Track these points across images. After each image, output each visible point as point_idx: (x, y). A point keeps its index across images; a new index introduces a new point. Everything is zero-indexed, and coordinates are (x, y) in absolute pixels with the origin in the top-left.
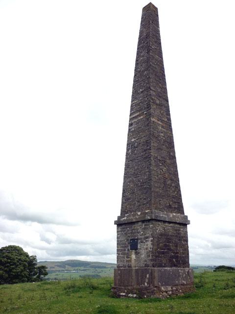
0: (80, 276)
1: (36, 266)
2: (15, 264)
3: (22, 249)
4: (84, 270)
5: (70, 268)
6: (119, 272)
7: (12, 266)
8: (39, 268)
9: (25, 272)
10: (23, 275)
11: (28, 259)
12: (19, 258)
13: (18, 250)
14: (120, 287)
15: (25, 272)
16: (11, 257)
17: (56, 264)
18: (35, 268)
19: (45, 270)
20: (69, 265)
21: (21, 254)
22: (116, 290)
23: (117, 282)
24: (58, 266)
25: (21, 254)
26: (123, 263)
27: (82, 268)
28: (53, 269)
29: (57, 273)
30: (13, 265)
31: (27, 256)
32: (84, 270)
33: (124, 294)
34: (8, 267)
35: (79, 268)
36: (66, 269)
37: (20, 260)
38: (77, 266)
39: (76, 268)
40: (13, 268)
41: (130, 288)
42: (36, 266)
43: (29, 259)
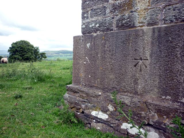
0: (68, 59)
1: (39, 53)
2: (25, 52)
3: (29, 43)
4: (70, 56)
5: (62, 54)
6: (88, 45)
7: (24, 53)
8: (41, 54)
9: (33, 56)
10: (31, 58)
11: (33, 49)
12: (28, 48)
13: (26, 43)
14: (91, 91)
15: (33, 56)
16: (23, 48)
17: (54, 52)
18: (38, 54)
19: (45, 55)
20: (62, 53)
21: (29, 46)
22: (77, 98)
23: (82, 75)
24: (55, 53)
25: (29, 46)
26: (100, 18)
27: (69, 54)
28: (53, 55)
29: (55, 57)
30: (24, 52)
31: (33, 47)
32: (70, 56)
33: (104, 116)
34: (21, 53)
35: (67, 54)
36: (60, 55)
37: (28, 49)
38: (66, 53)
39: (65, 54)
40: (25, 54)
41: (127, 100)
42: (39, 53)
43: (34, 48)
